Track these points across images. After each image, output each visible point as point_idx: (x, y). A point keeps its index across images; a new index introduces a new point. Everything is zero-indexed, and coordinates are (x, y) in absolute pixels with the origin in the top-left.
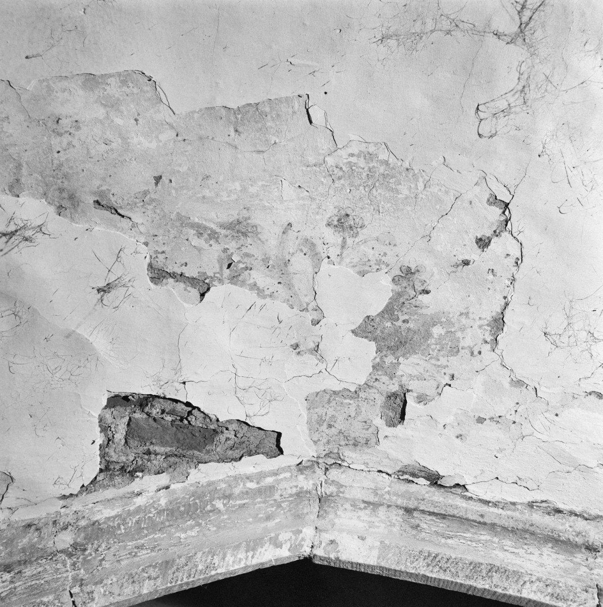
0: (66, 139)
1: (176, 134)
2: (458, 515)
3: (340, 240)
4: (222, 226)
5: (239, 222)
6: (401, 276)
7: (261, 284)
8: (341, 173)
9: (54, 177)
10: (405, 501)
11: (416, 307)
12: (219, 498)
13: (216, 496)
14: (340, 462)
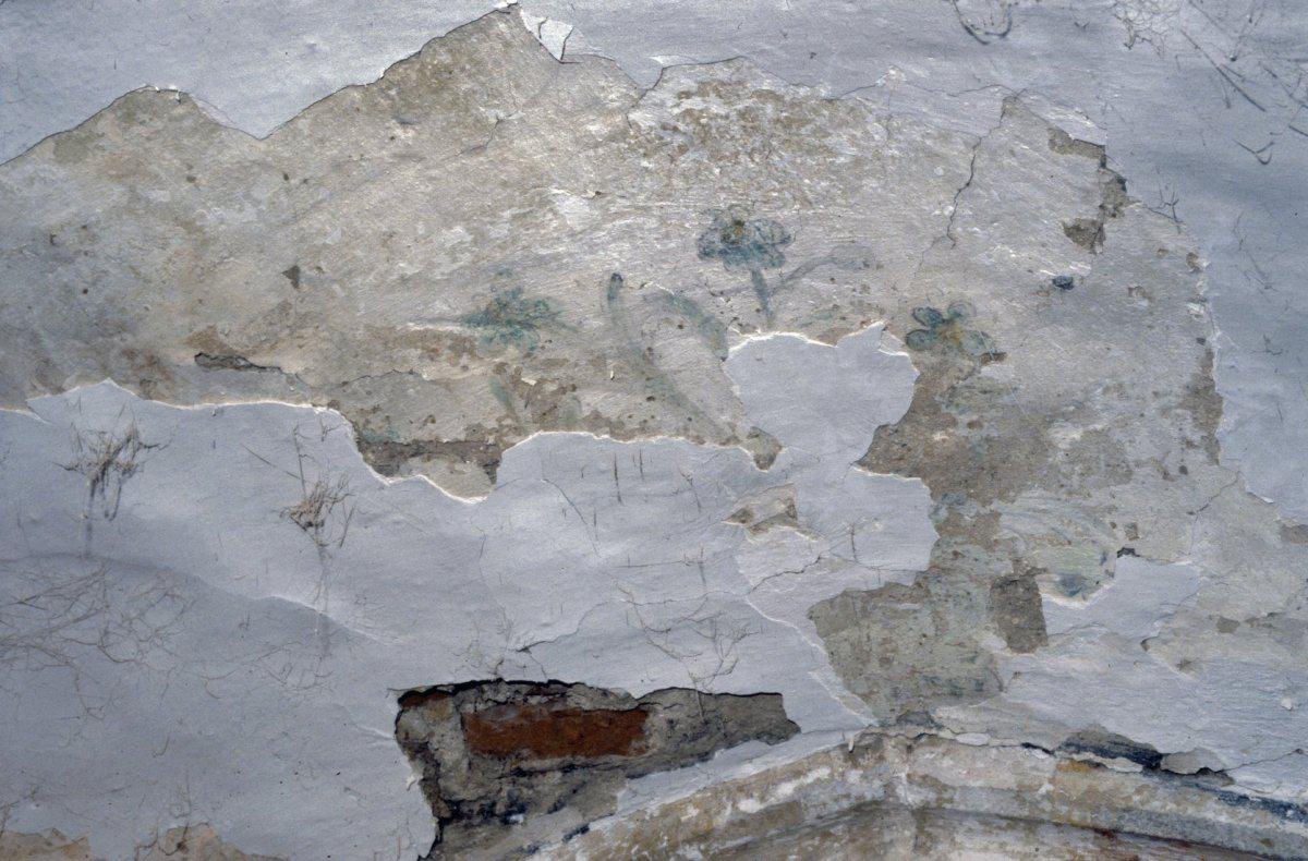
0: (84, 266)
1: (282, 177)
2: (1212, 843)
3: (745, 279)
4: (469, 320)
5: (504, 306)
6: (924, 331)
7: (611, 412)
8: (679, 140)
9: (102, 335)
10: (1088, 815)
11: (985, 392)
12: (689, 842)
13: (681, 837)
14: (934, 731)
